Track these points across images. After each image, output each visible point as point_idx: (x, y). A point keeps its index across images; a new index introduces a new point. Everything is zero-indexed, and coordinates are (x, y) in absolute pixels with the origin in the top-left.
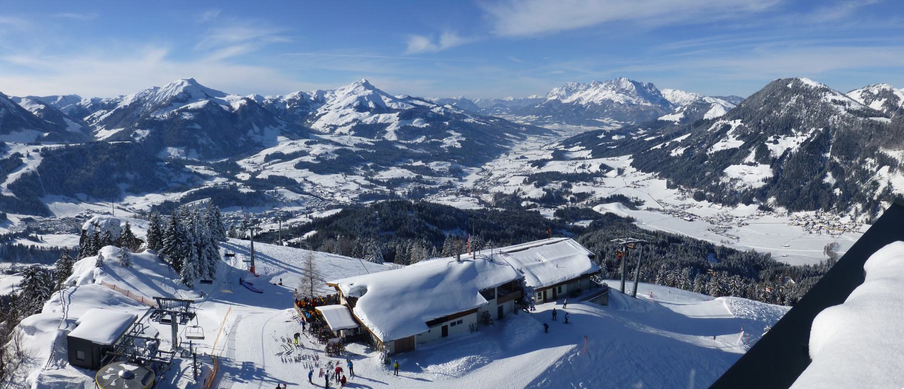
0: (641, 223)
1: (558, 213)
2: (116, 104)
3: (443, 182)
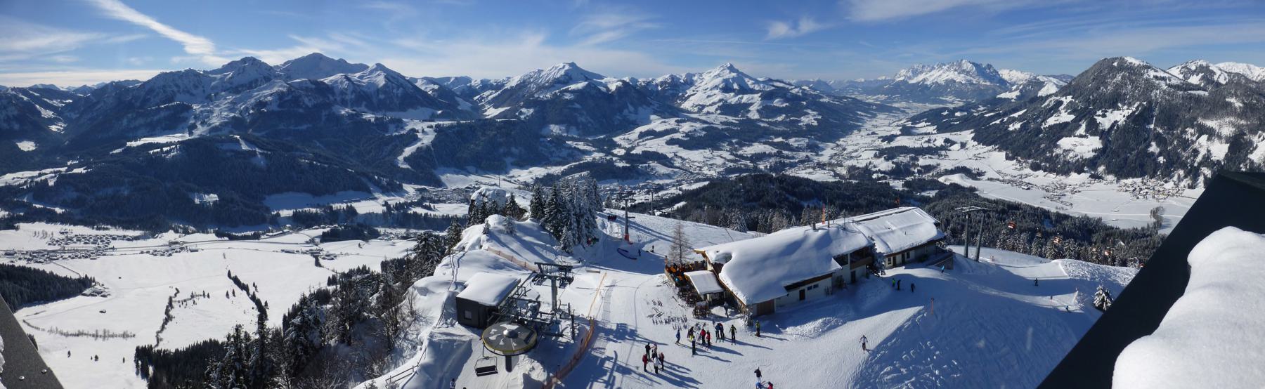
0: (982, 192)
1: (906, 184)
2: (503, 85)
3: (801, 157)
